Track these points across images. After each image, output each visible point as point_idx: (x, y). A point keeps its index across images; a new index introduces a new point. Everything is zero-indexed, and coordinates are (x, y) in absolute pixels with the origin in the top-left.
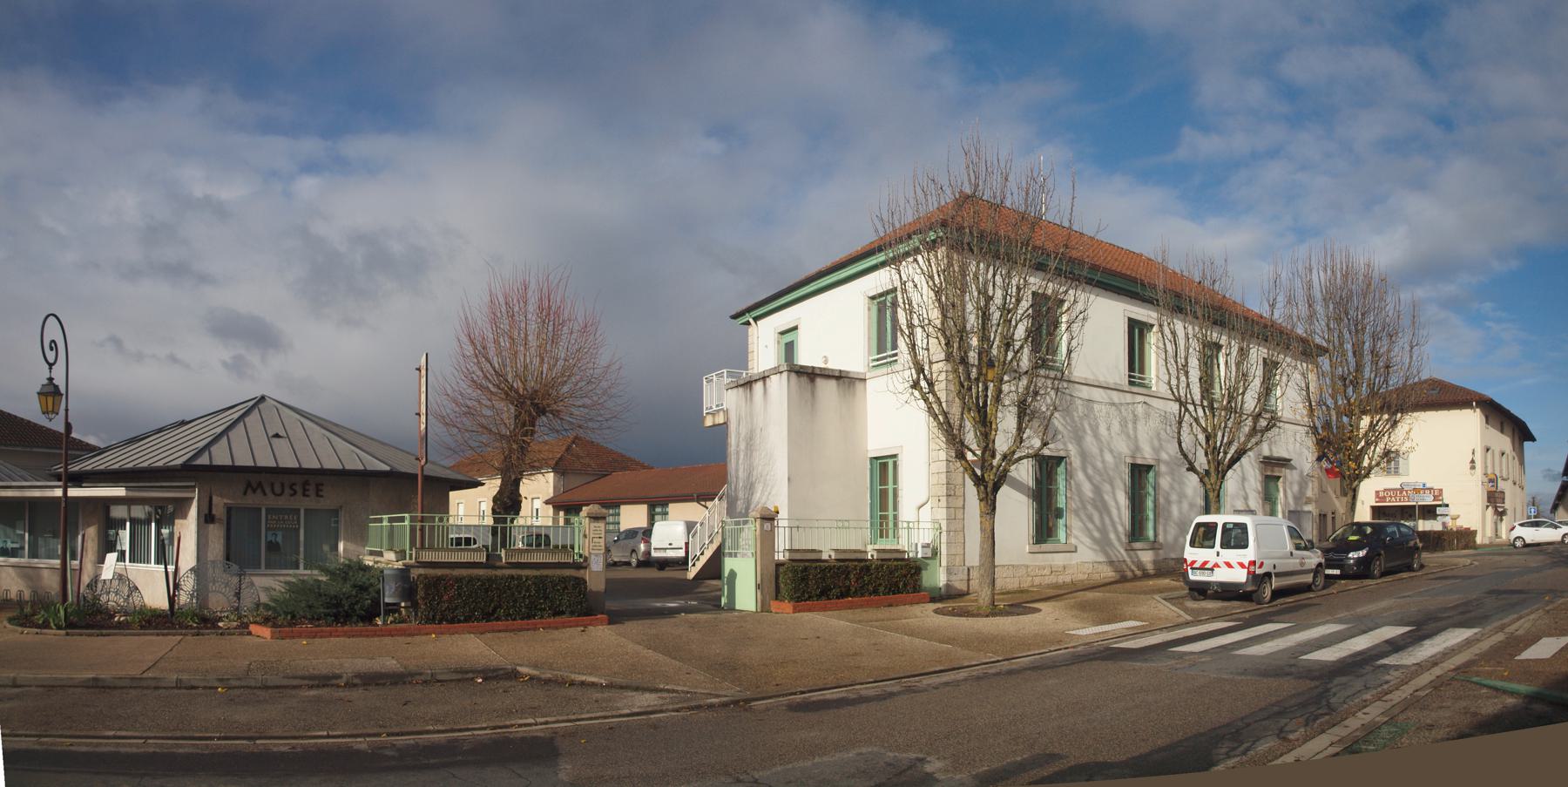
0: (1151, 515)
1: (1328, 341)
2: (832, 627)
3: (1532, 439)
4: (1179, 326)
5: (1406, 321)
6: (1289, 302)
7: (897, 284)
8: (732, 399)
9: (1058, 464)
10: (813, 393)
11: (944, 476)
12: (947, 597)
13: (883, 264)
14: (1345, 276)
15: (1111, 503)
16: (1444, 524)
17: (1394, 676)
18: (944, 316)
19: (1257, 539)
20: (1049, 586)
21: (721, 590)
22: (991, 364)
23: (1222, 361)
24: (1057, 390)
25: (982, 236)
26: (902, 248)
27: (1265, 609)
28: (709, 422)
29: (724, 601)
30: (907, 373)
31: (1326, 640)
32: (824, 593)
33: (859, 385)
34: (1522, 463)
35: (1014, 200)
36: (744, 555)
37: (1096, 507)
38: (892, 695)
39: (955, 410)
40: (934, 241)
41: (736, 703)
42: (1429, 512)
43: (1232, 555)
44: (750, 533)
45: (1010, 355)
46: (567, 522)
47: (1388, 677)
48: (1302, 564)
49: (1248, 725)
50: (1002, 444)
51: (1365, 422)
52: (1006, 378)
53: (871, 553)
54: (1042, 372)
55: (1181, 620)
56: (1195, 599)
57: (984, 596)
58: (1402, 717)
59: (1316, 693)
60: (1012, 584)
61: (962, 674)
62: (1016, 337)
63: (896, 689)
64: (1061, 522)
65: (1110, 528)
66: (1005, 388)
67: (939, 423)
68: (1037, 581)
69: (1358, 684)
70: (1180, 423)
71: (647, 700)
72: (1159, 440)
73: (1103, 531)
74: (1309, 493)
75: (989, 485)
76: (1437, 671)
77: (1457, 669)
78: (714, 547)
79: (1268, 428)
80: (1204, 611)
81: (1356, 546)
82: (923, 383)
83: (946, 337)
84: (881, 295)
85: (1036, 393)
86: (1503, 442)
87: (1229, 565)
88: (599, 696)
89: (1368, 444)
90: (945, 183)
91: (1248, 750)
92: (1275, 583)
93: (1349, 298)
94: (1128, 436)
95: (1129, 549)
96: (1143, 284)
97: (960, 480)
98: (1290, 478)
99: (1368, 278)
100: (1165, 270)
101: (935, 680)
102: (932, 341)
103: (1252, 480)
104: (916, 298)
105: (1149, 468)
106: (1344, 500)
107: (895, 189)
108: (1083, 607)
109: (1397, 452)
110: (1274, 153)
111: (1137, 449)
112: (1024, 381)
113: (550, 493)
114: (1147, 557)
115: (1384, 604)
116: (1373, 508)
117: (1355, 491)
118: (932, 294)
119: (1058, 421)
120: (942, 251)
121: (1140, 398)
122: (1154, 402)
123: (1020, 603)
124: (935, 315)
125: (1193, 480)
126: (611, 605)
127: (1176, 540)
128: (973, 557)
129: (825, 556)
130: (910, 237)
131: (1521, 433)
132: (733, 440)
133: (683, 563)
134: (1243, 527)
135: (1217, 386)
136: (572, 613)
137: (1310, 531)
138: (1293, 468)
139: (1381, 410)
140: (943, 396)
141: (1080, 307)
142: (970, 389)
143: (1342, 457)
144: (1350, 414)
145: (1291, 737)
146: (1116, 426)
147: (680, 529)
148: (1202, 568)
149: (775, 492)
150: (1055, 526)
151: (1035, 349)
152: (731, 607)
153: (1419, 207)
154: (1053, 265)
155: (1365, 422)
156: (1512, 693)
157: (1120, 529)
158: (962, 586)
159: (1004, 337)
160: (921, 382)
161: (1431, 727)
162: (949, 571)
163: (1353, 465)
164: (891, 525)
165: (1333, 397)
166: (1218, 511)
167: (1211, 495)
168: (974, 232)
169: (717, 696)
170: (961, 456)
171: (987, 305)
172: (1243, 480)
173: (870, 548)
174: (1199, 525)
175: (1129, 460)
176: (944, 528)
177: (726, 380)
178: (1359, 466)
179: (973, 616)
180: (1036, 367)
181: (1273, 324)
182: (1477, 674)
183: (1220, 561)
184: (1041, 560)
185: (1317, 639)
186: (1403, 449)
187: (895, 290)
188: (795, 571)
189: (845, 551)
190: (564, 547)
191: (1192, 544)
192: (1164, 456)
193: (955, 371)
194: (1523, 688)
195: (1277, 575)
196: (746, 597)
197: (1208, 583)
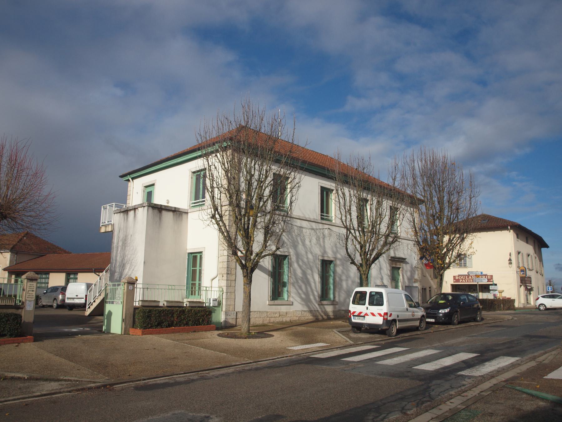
0: (332, 287)
1: (424, 197)
2: (162, 343)
3: (546, 246)
4: (346, 190)
6: (403, 177)
7: (207, 166)
8: (117, 219)
9: (284, 259)
11: (226, 264)
12: (226, 328)
13: (200, 157)
14: (432, 163)
16: (495, 295)
18: (229, 183)
19: (388, 301)
20: (278, 323)
21: (103, 322)
22: (252, 208)
23: (368, 207)
24: (285, 221)
25: (249, 145)
28: (103, 230)
30: (209, 211)
31: (429, 359)
32: (160, 324)
33: (184, 216)
34: (541, 260)
35: (265, 129)
36: (117, 303)
37: (303, 282)
38: (193, 380)
39: (233, 230)
40: (226, 147)
41: (105, 386)
42: (485, 288)
43: (375, 309)
44: (121, 290)
45: (261, 204)
46: (16, 281)
47: (464, 383)
48: (413, 315)
49: (384, 404)
50: (256, 248)
51: (446, 239)
52: (259, 215)
53: (186, 303)
54: (277, 212)
55: (347, 343)
56: (355, 332)
57: (244, 328)
58: (473, 407)
59: (424, 388)
60: (259, 321)
61: (231, 370)
62: (265, 195)
63: (196, 377)
64: (285, 289)
65: (310, 293)
66: (259, 220)
67: (224, 236)
68: (272, 320)
69: (447, 385)
70: (347, 239)
71: (54, 386)
72: (336, 247)
73: (307, 294)
74: (416, 277)
75: (249, 268)
76: (494, 381)
77: (506, 381)
78: (101, 298)
79: (393, 242)
80: (360, 339)
81: (443, 307)
82: (217, 216)
83: (229, 193)
84: (198, 171)
85: (274, 223)
86: (529, 249)
87: (373, 314)
88: (22, 385)
89: (448, 250)
91: (384, 418)
92: (398, 325)
93: (435, 174)
94: (320, 245)
95: (321, 305)
96: (328, 170)
97: (234, 266)
98: (406, 268)
99: (445, 164)
100: (339, 163)
101: (216, 373)
102: (223, 195)
103: (385, 269)
104: (215, 174)
105: (331, 262)
106: (436, 280)
107: (209, 120)
109: (465, 255)
110: (393, 106)
112: (268, 217)
113: (7, 264)
114: (329, 309)
115: (460, 340)
116: (452, 285)
118: (224, 172)
119: (285, 237)
120: (229, 152)
121: (327, 226)
122: (334, 228)
123: (263, 332)
124: (225, 182)
125: (354, 268)
126: (36, 330)
127: (345, 300)
128: (239, 307)
129: (161, 304)
130: (214, 144)
131: (539, 243)
132: (115, 240)
133: (83, 307)
135: (366, 221)
136: (11, 335)
137: (417, 297)
138: (407, 263)
139: (455, 232)
140: (227, 223)
141: (297, 181)
142: (241, 220)
143: (434, 258)
144: (437, 235)
145: (409, 412)
146: (314, 241)
147: (83, 287)
148: (359, 315)
149: (137, 270)
150: (282, 291)
151: (274, 201)
152: (108, 332)
153: (472, 126)
154: (284, 160)
155: (446, 239)
156: (543, 399)
157: (316, 293)
159: (258, 195)
161: (491, 414)
162: (226, 314)
163: (440, 262)
164: (197, 288)
165: (428, 225)
166: (367, 285)
167: (363, 277)
168: (245, 144)
169: (94, 382)
170: (235, 254)
171: (251, 179)
172: (380, 269)
173: (185, 300)
174: (357, 293)
175: (321, 258)
176: (225, 291)
177: (114, 209)
178: (444, 262)
180: (274, 210)
181: (395, 189)
182: (520, 385)
183: (368, 312)
184: (274, 309)
185: (422, 358)
186: (468, 253)
187: (205, 169)
189: (172, 302)
190: (10, 296)
191: (354, 303)
192: (339, 256)
193: (234, 210)
194: (550, 397)
195: (400, 321)
196: (116, 326)
197: (362, 324)
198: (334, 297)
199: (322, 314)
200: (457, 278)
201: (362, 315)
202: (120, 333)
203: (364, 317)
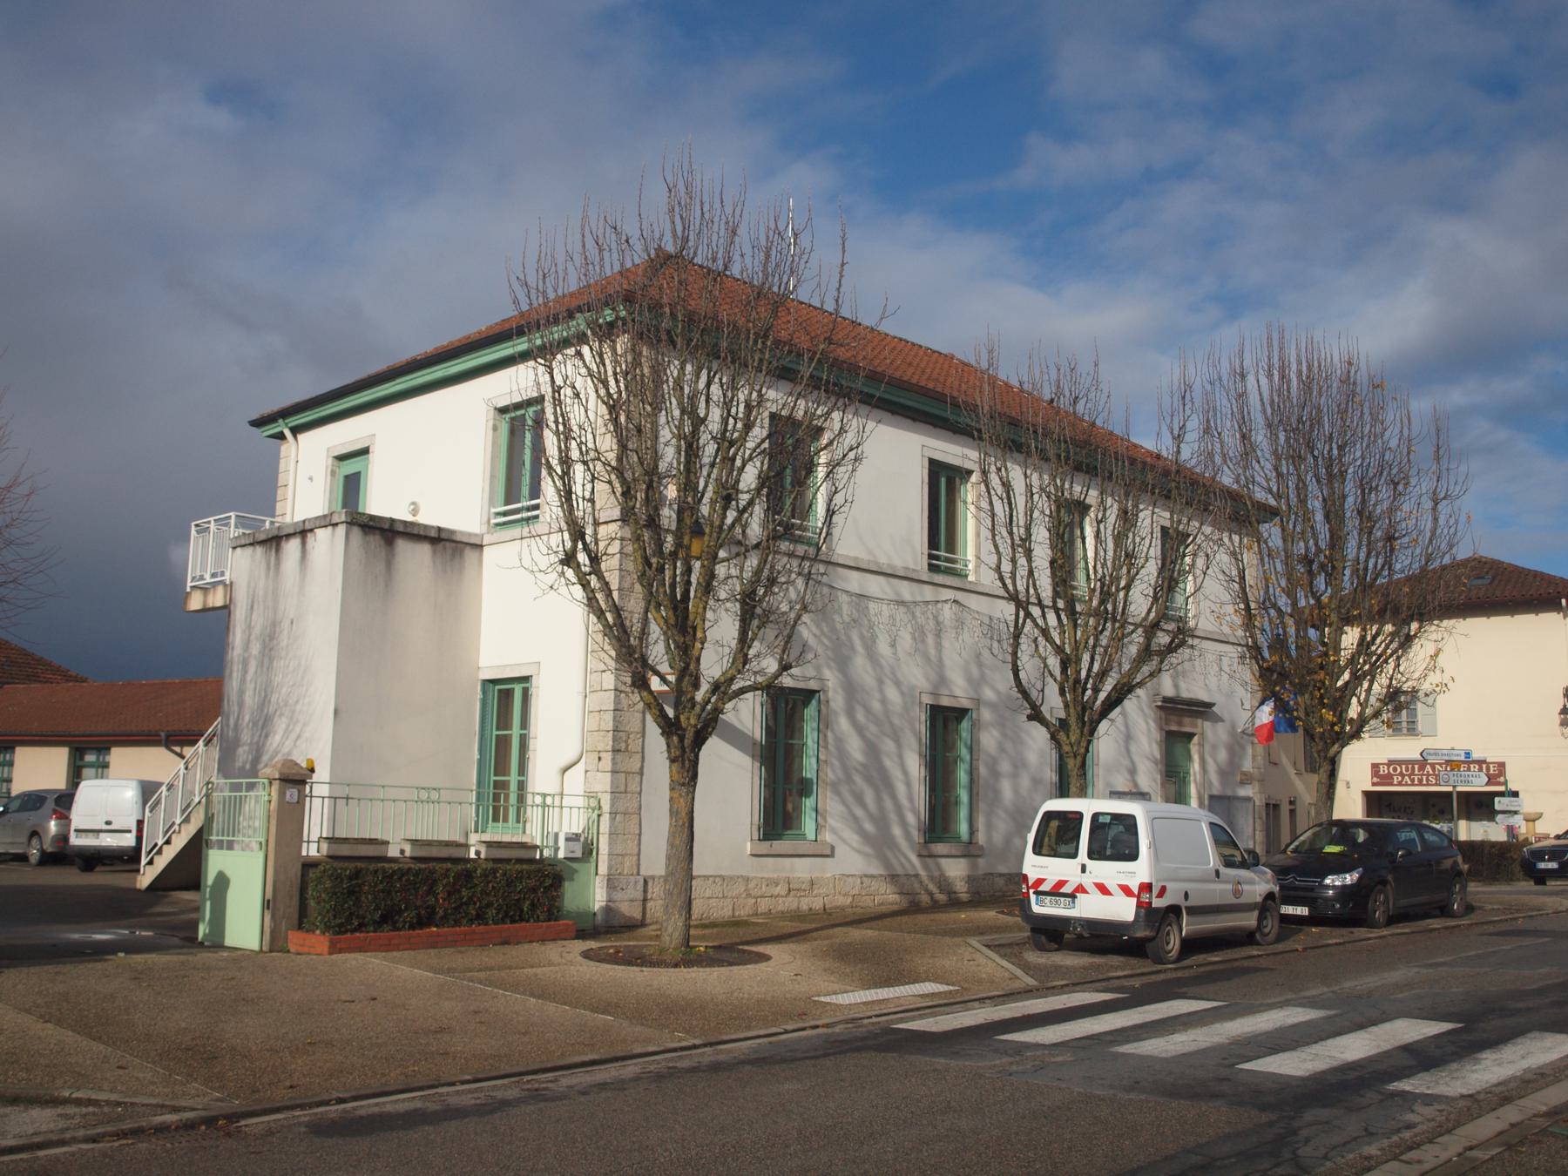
0: (964, 796)
1: (1278, 497)
2: (398, 978)
4: (1016, 474)
5: (1423, 451)
6: (1207, 431)
7: (547, 390)
8: (243, 566)
9: (806, 703)
10: (389, 564)
11: (609, 717)
12: (607, 929)
13: (524, 357)
14: (1307, 385)
15: (896, 774)
16: (1511, 830)
17: (1421, 1116)
18: (623, 447)
19: (1153, 845)
20: (783, 916)
21: (198, 909)
22: (698, 531)
23: (1089, 531)
25: (691, 319)
26: (557, 333)
27: (1169, 972)
28: (195, 603)
29: (203, 930)
30: (555, 539)
31: (1293, 1039)
32: (388, 919)
33: (470, 555)
35: (745, 265)
36: (245, 848)
37: (868, 779)
38: (505, 1104)
39: (634, 605)
40: (611, 325)
41: (210, 1121)
42: (1480, 806)
43: (1110, 871)
44: (259, 804)
45: (731, 516)
47: (1410, 1117)
48: (1237, 893)
50: (712, 664)
51: (1350, 638)
52: (722, 554)
54: (784, 546)
55: (1017, 985)
56: (1042, 949)
57: (672, 930)
60: (721, 910)
61: (631, 1069)
63: (512, 1093)
64: (808, 803)
65: (893, 817)
66: (721, 570)
67: (607, 626)
68: (764, 905)
70: (1017, 636)
71: (40, 1120)
72: (980, 665)
73: (881, 821)
74: (1247, 765)
75: (688, 735)
76: (1511, 1114)
77: (1553, 1113)
79: (1171, 649)
81: (1339, 865)
82: (582, 557)
83: (623, 481)
84: (517, 406)
85: (772, 581)
87: (1103, 889)
89: (1357, 678)
90: (634, 233)
92: (1188, 926)
93: (1317, 421)
96: (955, 405)
100: (993, 381)
102: (601, 487)
104: (576, 415)
105: (961, 713)
106: (1315, 778)
108: (845, 954)
109: (1414, 692)
110: (1184, 170)
111: (942, 680)
112: (753, 561)
114: (956, 870)
115: (1398, 975)
116: (1368, 795)
117: (1333, 764)
118: (603, 410)
119: (807, 630)
120: (622, 343)
121: (948, 594)
122: (973, 602)
123: (734, 943)
124: (607, 444)
125: (1038, 736)
127: (1008, 841)
128: (655, 860)
129: (393, 852)
130: (571, 316)
132: (237, 637)
133: (129, 859)
134: (1128, 822)
135: (1081, 576)
137: (1250, 835)
138: (1217, 719)
139: (1380, 616)
140: (614, 580)
141: (850, 439)
142: (661, 570)
143: (1310, 700)
146: (906, 640)
147: (129, 794)
149: (311, 737)
150: (798, 809)
151: (773, 508)
152: (216, 943)
154: (806, 370)
155: (1350, 638)
157: (911, 819)
158: (631, 910)
159: (721, 485)
160: (579, 556)
162: (612, 884)
163: (1329, 716)
164: (513, 798)
165: (1290, 593)
166: (1082, 793)
167: (1071, 763)
168: (673, 313)
169: (176, 1110)
170: (641, 683)
174: (1049, 816)
176: (606, 807)
177: (233, 531)
179: (652, 964)
180: (774, 537)
183: (1087, 881)
186: (1426, 686)
187: (540, 400)
188: (337, 878)
189: (429, 843)
191: (1038, 850)
192: (988, 694)
193: (638, 538)
196: (244, 925)
198: (972, 831)
199: (931, 887)
200: (1383, 770)
201: (1066, 889)
202: (255, 946)
203: (1072, 896)
